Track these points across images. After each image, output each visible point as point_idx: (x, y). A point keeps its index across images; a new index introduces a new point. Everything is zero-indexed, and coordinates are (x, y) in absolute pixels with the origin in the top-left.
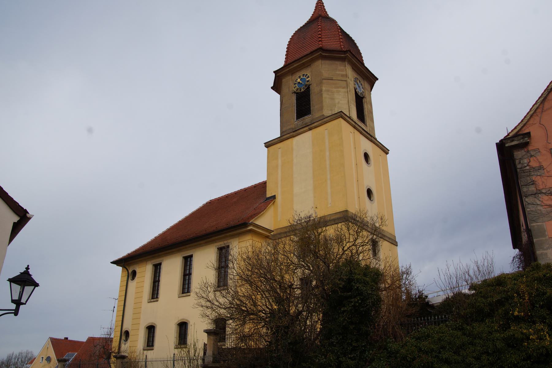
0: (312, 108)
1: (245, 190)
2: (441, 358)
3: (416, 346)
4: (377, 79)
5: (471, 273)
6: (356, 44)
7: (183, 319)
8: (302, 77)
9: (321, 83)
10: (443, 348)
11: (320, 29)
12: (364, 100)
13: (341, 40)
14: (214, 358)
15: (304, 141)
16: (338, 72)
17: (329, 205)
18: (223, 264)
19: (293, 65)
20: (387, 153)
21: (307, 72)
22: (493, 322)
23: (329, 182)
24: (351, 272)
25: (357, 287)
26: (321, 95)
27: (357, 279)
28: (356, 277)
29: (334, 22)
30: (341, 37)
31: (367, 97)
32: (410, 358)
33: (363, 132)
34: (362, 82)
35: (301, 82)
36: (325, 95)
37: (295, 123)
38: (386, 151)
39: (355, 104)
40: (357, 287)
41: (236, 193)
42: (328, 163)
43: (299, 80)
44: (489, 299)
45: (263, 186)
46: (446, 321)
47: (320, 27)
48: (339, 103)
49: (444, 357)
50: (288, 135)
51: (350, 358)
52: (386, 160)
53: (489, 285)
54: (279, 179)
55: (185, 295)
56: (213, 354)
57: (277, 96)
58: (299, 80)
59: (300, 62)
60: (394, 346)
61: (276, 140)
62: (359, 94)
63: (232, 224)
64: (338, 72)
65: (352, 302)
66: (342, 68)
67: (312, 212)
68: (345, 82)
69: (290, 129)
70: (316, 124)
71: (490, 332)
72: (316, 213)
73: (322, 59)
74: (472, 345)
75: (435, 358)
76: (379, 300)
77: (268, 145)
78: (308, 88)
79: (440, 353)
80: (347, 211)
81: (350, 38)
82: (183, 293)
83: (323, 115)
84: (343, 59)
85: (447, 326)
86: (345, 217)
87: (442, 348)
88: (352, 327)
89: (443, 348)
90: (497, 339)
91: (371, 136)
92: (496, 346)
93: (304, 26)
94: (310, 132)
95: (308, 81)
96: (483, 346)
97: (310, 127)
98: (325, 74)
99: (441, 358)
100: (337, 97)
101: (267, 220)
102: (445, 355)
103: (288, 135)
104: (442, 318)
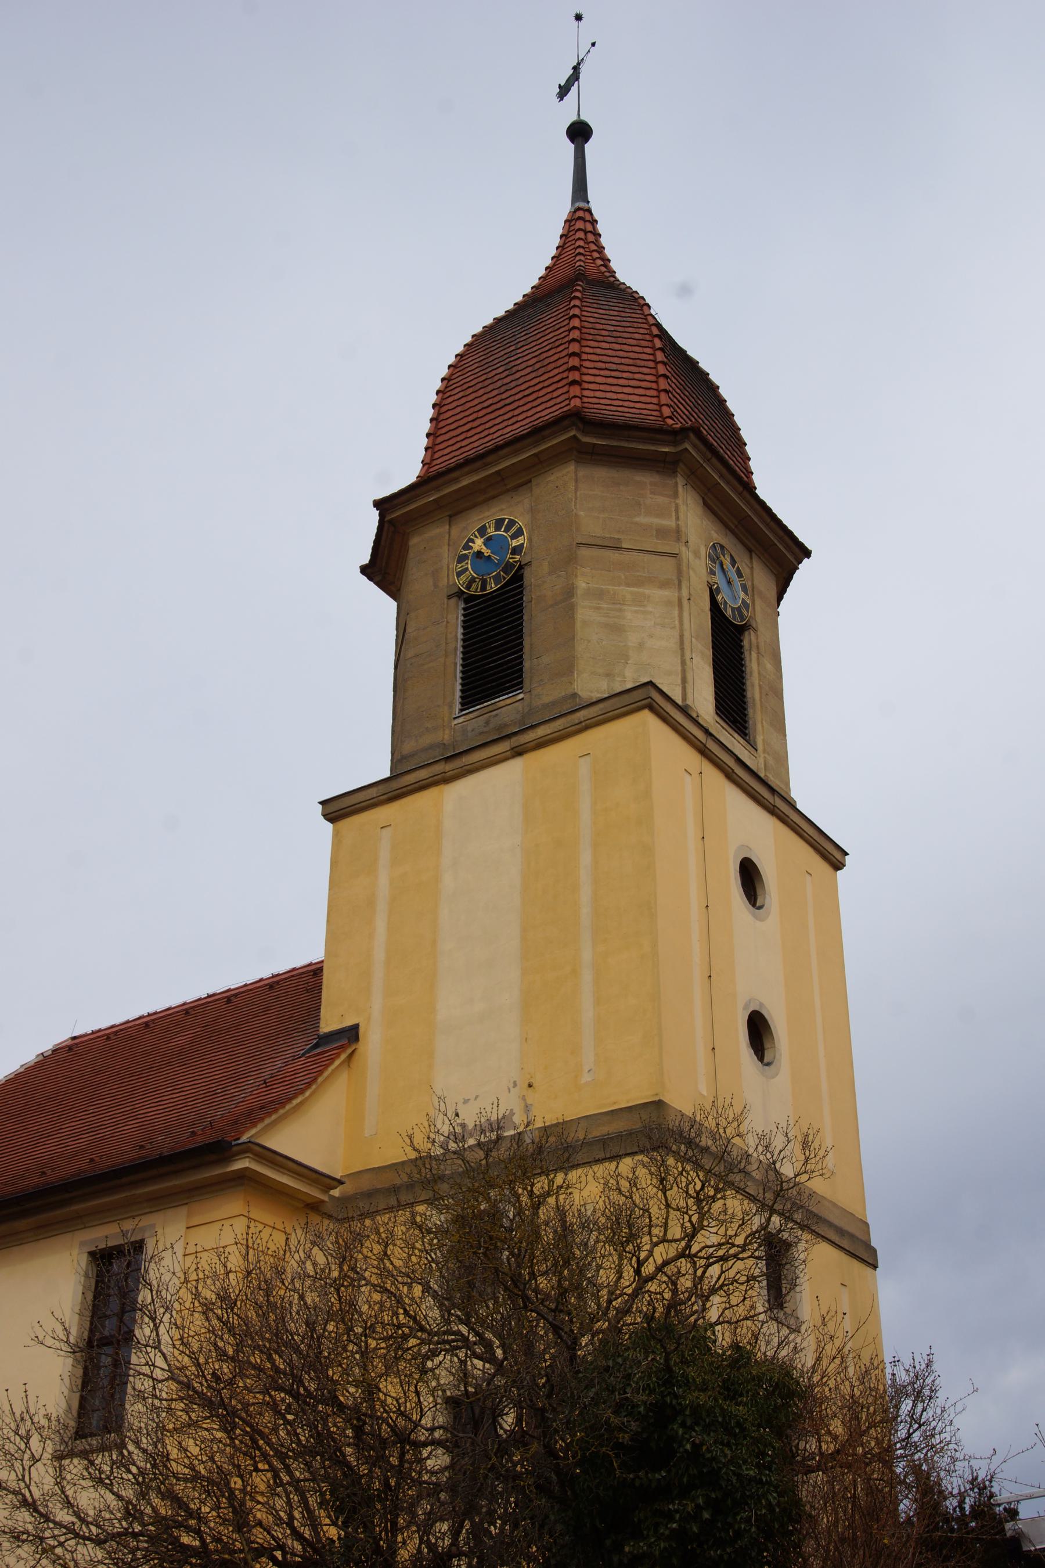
0: (527, 665)
1: (229, 1000)
4: (807, 553)
6: (722, 402)
8: (491, 531)
9: (568, 561)
11: (575, 334)
12: (748, 640)
15: (489, 803)
16: (643, 519)
17: (586, 1078)
18: (109, 1327)
19: (456, 480)
21: (515, 510)
23: (587, 976)
29: (635, 303)
30: (661, 369)
31: (761, 629)
34: (743, 564)
35: (486, 552)
36: (585, 612)
37: (451, 720)
38: (833, 856)
39: (709, 653)
42: (585, 895)
43: (479, 544)
45: (310, 978)
47: (576, 322)
48: (641, 646)
50: (423, 774)
54: (379, 954)
58: (479, 544)
59: (486, 466)
61: (373, 792)
62: (729, 613)
63: (164, 1144)
64: (643, 519)
65: (669, 1516)
67: (510, 1103)
68: (671, 561)
69: (432, 747)
70: (541, 732)
72: (527, 1108)
77: (337, 810)
78: (516, 579)
80: (659, 1105)
83: (575, 695)
84: (665, 466)
91: (772, 790)
93: (510, 314)
94: (516, 765)
95: (516, 550)
97: (514, 740)
101: (320, 1134)
103: (423, 774)
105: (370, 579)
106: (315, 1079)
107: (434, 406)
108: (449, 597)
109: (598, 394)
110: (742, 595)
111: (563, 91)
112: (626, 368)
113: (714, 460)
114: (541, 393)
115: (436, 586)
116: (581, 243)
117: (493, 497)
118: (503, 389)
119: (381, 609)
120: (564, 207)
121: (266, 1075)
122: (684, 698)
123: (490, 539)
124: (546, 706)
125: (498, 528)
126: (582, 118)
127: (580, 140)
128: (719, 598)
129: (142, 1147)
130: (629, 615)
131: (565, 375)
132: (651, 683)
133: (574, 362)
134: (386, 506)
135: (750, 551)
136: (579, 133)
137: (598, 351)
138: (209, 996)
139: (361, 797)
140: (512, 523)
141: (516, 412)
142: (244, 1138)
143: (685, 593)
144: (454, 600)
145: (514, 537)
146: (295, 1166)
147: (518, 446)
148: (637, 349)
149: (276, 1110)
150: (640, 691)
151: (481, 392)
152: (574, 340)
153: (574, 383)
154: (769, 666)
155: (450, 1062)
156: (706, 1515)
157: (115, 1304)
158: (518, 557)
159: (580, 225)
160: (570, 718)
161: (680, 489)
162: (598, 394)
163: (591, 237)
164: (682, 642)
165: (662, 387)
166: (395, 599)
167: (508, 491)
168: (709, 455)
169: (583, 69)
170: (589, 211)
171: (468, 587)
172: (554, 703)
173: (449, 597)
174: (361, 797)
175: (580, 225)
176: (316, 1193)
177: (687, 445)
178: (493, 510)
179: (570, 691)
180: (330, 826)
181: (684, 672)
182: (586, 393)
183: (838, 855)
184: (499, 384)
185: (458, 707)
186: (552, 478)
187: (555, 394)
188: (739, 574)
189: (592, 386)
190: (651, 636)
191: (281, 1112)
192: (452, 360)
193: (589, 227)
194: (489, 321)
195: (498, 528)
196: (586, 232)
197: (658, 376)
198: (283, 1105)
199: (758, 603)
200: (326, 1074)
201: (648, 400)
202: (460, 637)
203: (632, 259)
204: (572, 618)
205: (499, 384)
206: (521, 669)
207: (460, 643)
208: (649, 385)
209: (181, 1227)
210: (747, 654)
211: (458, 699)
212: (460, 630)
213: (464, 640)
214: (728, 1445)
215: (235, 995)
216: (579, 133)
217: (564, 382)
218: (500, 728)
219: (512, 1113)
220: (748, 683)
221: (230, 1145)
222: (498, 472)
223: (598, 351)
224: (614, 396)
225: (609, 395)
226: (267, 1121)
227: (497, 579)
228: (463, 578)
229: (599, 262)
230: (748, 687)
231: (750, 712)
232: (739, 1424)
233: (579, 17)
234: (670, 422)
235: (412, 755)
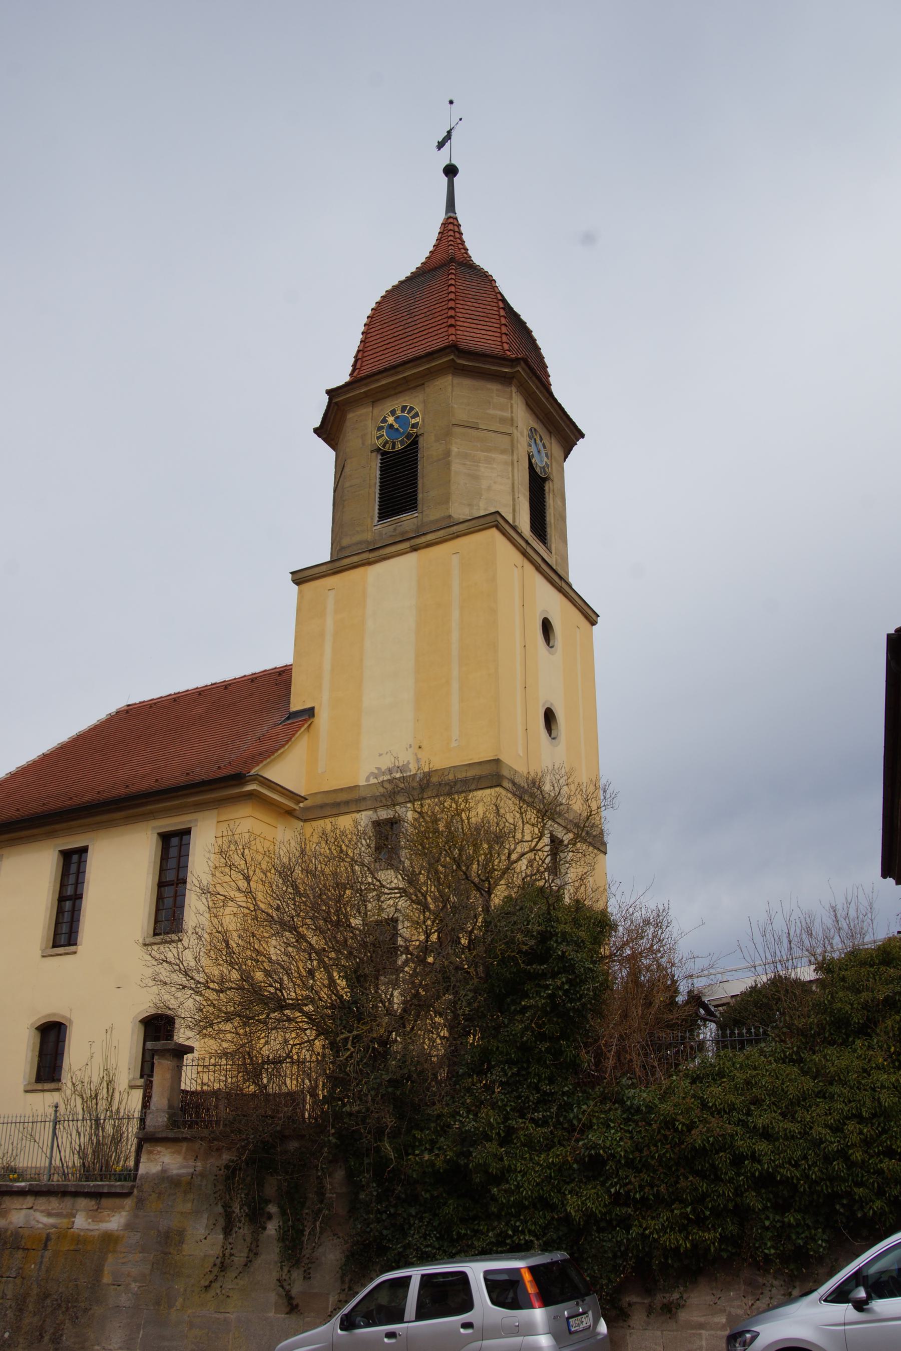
0: (420, 496)
1: (226, 687)
2: (751, 1125)
3: (694, 1096)
4: (582, 435)
5: (818, 930)
6: (534, 341)
7: (54, 1015)
8: (399, 413)
9: (447, 434)
10: (756, 1102)
11: (452, 296)
12: (548, 486)
13: (504, 330)
14: (171, 1116)
15: (395, 579)
16: (491, 412)
17: (454, 744)
18: (170, 876)
19: (378, 380)
20: (593, 623)
21: (414, 401)
22: (870, 1047)
23: (455, 685)
24: (548, 918)
25: (563, 953)
26: (449, 464)
27: (564, 934)
28: (560, 928)
29: (486, 279)
30: (503, 321)
31: (555, 480)
32: (683, 1124)
33: (543, 566)
34: (546, 440)
35: (396, 426)
36: (456, 467)
37: (372, 527)
38: (591, 617)
39: (528, 494)
40: (563, 953)
41: (201, 693)
42: (455, 636)
43: (391, 420)
44: (864, 995)
45: (280, 678)
46: (758, 1042)
47: (452, 289)
48: (489, 488)
49: (760, 1122)
50: (355, 559)
51: (532, 1120)
52: (590, 637)
53: (863, 964)
54: (327, 666)
55: (61, 950)
56: (170, 1106)
57: (328, 455)
58: (391, 420)
59: (397, 373)
60: (640, 1096)
61: (324, 568)
62: (538, 470)
63: (201, 774)
64: (491, 412)
65: (547, 987)
66: (503, 400)
67: (406, 757)
68: (507, 439)
69: (360, 543)
70: (429, 537)
71: (865, 1070)
73: (453, 374)
74: (824, 1097)
75: (738, 1125)
76: (606, 986)
77: (301, 578)
78: (414, 443)
79: (749, 1114)
80: (497, 761)
81: (523, 324)
82: (54, 946)
83: (450, 517)
84: (505, 380)
85: (762, 1052)
86: (491, 774)
87: (754, 1104)
88: (544, 1046)
89: (756, 1102)
90: (883, 1086)
91: (561, 578)
92: (880, 1103)
93: (408, 279)
94: (413, 556)
95: (415, 426)
96: (850, 1102)
97: (413, 543)
98: (461, 413)
99: (751, 1125)
100: (481, 473)
101: (289, 770)
102: (761, 1121)
103: (355, 559)
104: (741, 1035)
105: (319, 436)
106: (291, 739)
107: (363, 333)
108: (372, 452)
109: (466, 333)
110: (545, 459)
111: (441, 145)
112: (482, 319)
113: (534, 378)
114: (430, 330)
115: (363, 444)
116: (451, 238)
117: (400, 392)
118: (406, 326)
119: (324, 456)
120: (440, 215)
121: (258, 735)
122: (514, 521)
123: (398, 418)
124: (432, 522)
125: (403, 411)
126: (453, 162)
127: (451, 175)
128: (533, 461)
129: (187, 774)
130: (482, 469)
131: (446, 320)
132: (497, 512)
133: (451, 313)
134: (334, 393)
135: (550, 433)
136: (451, 171)
137: (466, 307)
138: (212, 684)
139: (316, 570)
140: (412, 409)
141: (415, 341)
142: (252, 772)
143: (515, 458)
144: (374, 454)
145: (413, 417)
146: (281, 789)
147: (418, 362)
148: (488, 307)
149: (269, 756)
150: (491, 517)
151: (393, 327)
152: (451, 299)
153: (451, 326)
154: (559, 503)
155: (368, 734)
156: (566, 987)
157: (72, 879)
158: (415, 430)
159: (451, 227)
160: (447, 530)
161: (514, 395)
162: (466, 333)
163: (457, 235)
164: (513, 488)
165: (503, 331)
166: (333, 446)
167: (409, 389)
168: (531, 375)
169: (454, 133)
170: (456, 219)
171: (384, 446)
172: (437, 521)
173: (372, 452)
174: (316, 570)
175: (451, 227)
176: (292, 805)
177: (519, 369)
178: (401, 400)
179: (447, 514)
180: (295, 588)
181: (514, 505)
182: (458, 332)
183: (594, 616)
184: (404, 322)
185: (377, 519)
186: (437, 383)
187: (439, 332)
188: (544, 447)
189: (462, 328)
190: (495, 483)
191: (272, 757)
192: (374, 306)
193: (456, 229)
194: (396, 283)
195: (403, 411)
196: (454, 232)
197: (502, 325)
198: (273, 753)
199: (554, 464)
200: (297, 735)
201: (495, 339)
202: (378, 476)
203: (481, 251)
204: (449, 469)
205: (404, 322)
206: (416, 499)
207: (378, 480)
208: (495, 330)
209: (215, 821)
210: (547, 495)
211: (376, 515)
212: (378, 472)
213: (381, 479)
214: (577, 951)
215: (230, 685)
216: (451, 171)
217: (445, 325)
218: (403, 533)
219: (408, 763)
220: (547, 512)
221: (245, 776)
222: (404, 378)
223: (466, 307)
224: (475, 335)
225: (472, 334)
226: (265, 763)
227: (402, 442)
228: (381, 440)
229: (463, 251)
230: (548, 515)
231: (548, 530)
232: (583, 941)
233: (451, 102)
234: (508, 353)
235: (349, 547)
